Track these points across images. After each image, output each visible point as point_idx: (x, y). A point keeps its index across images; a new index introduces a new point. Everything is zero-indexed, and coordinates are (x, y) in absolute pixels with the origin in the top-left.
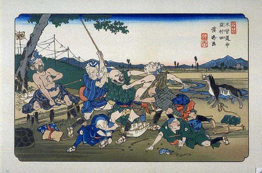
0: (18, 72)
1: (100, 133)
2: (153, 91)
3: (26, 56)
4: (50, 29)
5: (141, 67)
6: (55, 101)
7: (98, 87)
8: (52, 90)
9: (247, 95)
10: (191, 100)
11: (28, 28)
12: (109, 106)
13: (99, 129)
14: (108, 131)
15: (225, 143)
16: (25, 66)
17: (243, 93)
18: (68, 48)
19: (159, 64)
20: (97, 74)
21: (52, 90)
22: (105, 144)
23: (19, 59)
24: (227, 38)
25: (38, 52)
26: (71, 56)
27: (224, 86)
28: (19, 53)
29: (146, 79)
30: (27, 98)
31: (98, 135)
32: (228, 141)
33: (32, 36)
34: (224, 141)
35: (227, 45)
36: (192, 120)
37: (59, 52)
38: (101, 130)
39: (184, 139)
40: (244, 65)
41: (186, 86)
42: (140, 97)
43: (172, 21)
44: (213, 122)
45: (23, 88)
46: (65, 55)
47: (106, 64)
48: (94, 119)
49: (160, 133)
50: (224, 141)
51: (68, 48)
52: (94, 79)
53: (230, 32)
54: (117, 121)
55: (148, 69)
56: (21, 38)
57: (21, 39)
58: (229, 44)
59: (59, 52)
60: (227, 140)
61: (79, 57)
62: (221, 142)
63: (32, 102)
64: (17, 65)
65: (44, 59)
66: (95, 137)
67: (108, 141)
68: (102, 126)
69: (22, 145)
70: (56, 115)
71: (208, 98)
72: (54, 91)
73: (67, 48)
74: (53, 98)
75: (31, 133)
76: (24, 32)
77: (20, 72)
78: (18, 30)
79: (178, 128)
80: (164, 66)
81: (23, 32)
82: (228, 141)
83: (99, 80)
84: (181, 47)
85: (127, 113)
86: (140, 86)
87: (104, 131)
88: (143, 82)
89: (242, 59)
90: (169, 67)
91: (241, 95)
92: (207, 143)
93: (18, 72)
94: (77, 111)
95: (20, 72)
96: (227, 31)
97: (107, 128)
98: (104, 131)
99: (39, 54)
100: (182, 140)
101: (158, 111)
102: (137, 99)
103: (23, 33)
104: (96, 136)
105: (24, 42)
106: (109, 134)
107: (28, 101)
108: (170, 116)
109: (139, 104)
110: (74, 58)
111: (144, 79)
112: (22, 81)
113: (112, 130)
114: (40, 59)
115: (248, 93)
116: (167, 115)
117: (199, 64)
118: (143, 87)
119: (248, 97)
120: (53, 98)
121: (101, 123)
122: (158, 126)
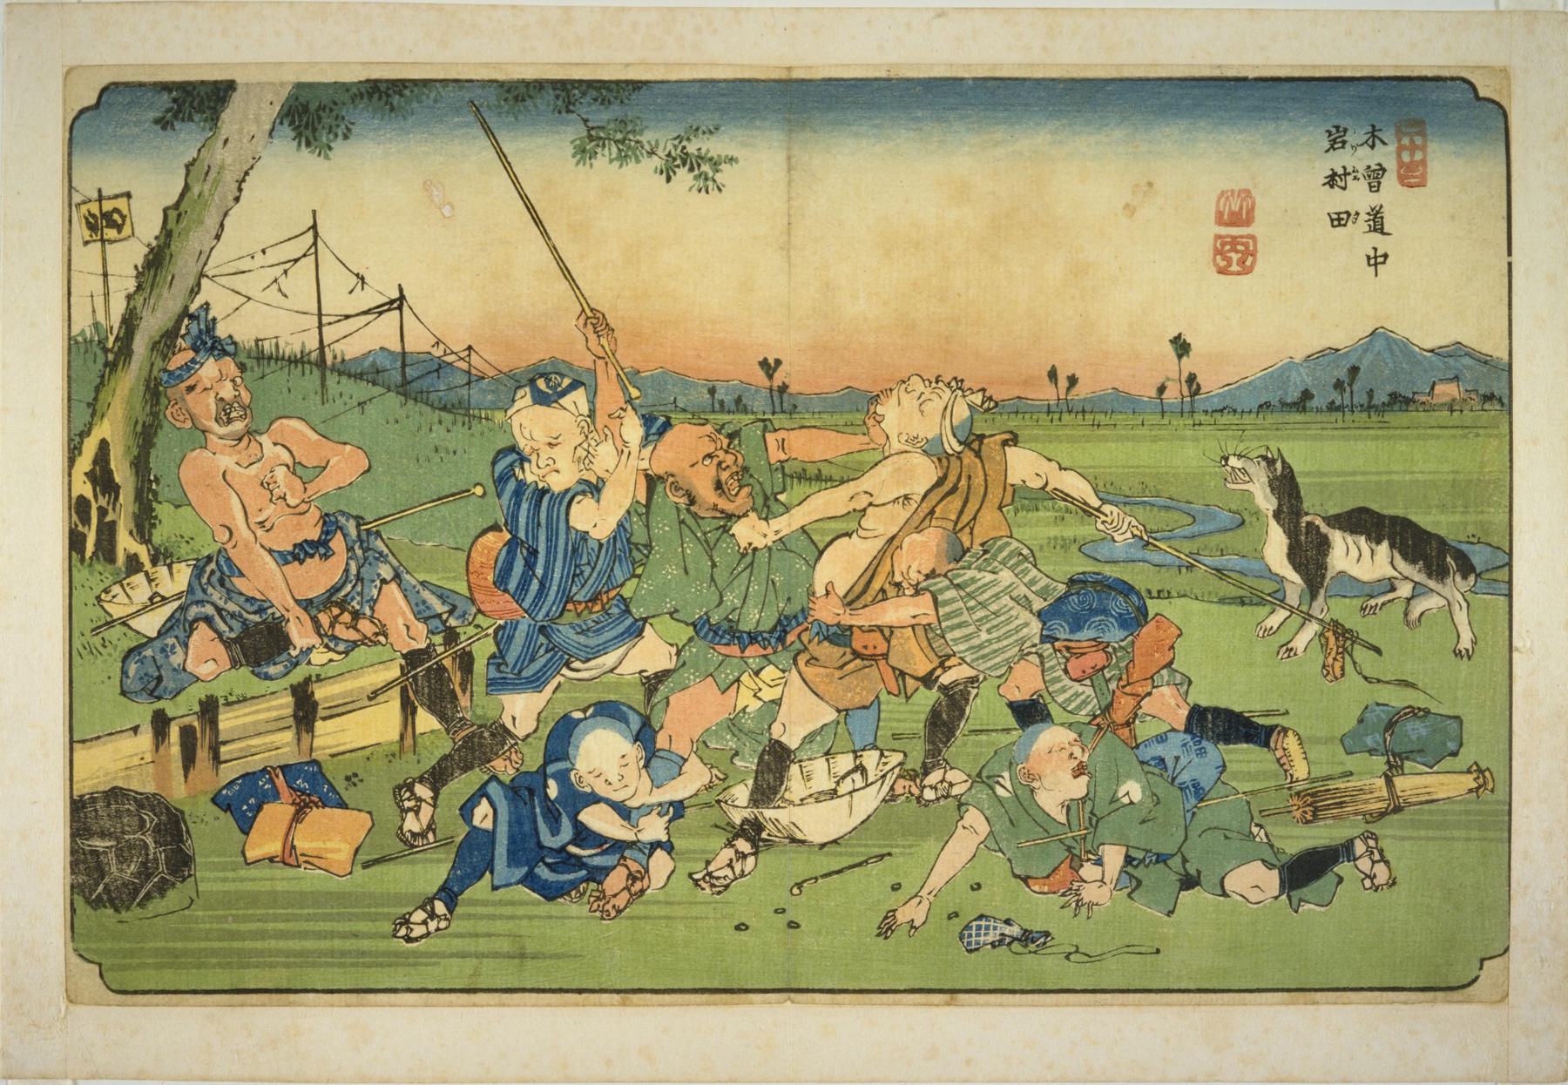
0: (90, 447)
1: (598, 819)
2: (921, 553)
3: (140, 345)
4: (283, 186)
5: (858, 405)
6: (317, 624)
7: (584, 536)
8: (301, 552)
9: (1502, 575)
10: (1153, 606)
11: (147, 183)
12: (652, 652)
13: (594, 799)
14: (647, 809)
15: (1367, 876)
16: (144, 375)
17: (1478, 557)
18: (401, 290)
19: (958, 384)
20: (581, 453)
21: (301, 552)
22: (627, 888)
23: (96, 359)
24: (1377, 222)
25: (214, 319)
26: (418, 341)
27: (1363, 522)
28: (224, 743)
29: (880, 482)
30: (142, 605)
31: (583, 835)
32: (1387, 863)
33: (175, 215)
34: (1364, 864)
35: (1376, 260)
36: (1161, 739)
37: (347, 317)
38: (608, 802)
39: (1113, 857)
40: (1486, 387)
41: (1121, 526)
42: (841, 593)
43: (1038, 124)
44: (1291, 742)
45: (126, 543)
46: (381, 334)
47: (635, 393)
48: (561, 736)
49: (967, 821)
50: (1364, 864)
51: (401, 290)
52: (558, 483)
53: (1390, 181)
54: (701, 746)
55: (902, 418)
56: (111, 233)
57: (111, 242)
58: (1386, 256)
59: (347, 317)
60: (1383, 860)
61: (470, 348)
62: (1343, 868)
63: (180, 626)
64: (84, 406)
65: (258, 360)
66: (573, 849)
67: (647, 871)
68: (614, 778)
69: (120, 898)
70: (328, 712)
71: (1254, 593)
72: (313, 563)
73: (396, 295)
74: (307, 605)
75: (172, 826)
76: (128, 195)
77: (1312, 397)
78: (86, 187)
79: (1079, 787)
80: (990, 399)
81: (122, 195)
82: (1387, 863)
83: (594, 489)
84: (1156, 272)
85: (768, 694)
86: (850, 523)
87: (624, 811)
88: (863, 502)
89: (1470, 353)
90: (1019, 407)
91: (1466, 568)
92: (1254, 881)
93: (90, 447)
94: (457, 678)
95: (104, 445)
96: (1375, 176)
97: (639, 791)
98: (624, 811)
99: (221, 331)
100: (1099, 862)
101: (955, 683)
102: (828, 612)
103: (121, 204)
104: (575, 841)
105: (127, 257)
106: (653, 828)
107: (150, 624)
108: (1029, 713)
109: (839, 635)
110: (437, 352)
111: (866, 483)
112: (113, 513)
113: (671, 804)
114: (229, 365)
115: (1510, 565)
116: (1011, 705)
117: (1210, 383)
118: (861, 528)
119: (1510, 582)
120: (307, 605)
121: (603, 755)
122: (952, 776)
